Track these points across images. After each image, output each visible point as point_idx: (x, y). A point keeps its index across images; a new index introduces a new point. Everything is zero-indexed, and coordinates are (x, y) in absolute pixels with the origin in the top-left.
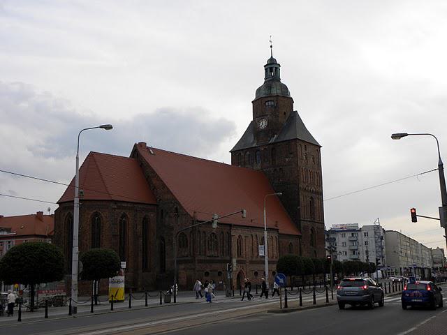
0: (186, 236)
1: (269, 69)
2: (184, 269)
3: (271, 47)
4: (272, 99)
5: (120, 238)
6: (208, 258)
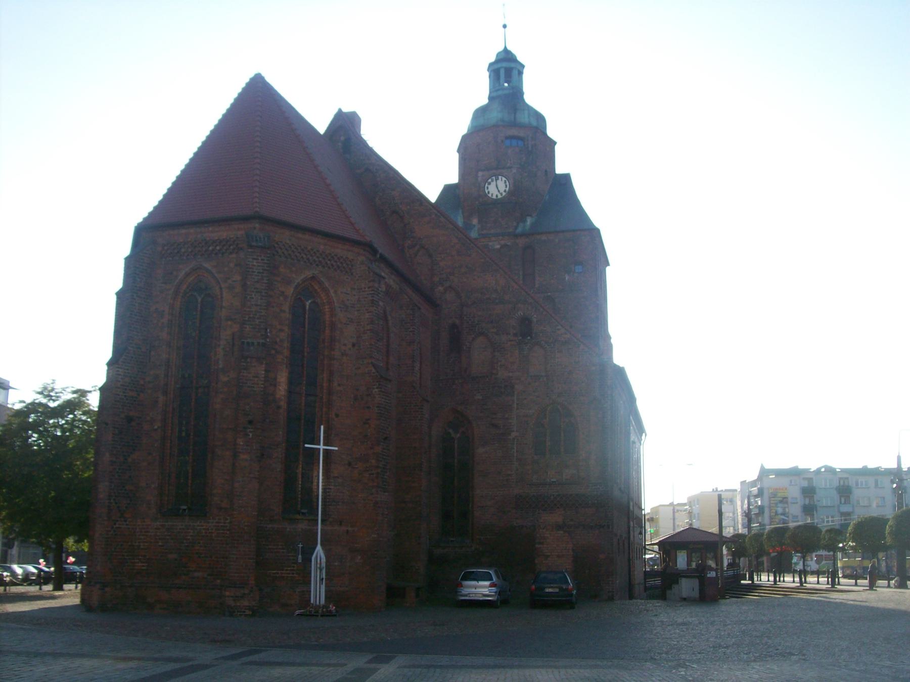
1: (502, 72)
2: (559, 527)
3: (505, 26)
4: (522, 134)
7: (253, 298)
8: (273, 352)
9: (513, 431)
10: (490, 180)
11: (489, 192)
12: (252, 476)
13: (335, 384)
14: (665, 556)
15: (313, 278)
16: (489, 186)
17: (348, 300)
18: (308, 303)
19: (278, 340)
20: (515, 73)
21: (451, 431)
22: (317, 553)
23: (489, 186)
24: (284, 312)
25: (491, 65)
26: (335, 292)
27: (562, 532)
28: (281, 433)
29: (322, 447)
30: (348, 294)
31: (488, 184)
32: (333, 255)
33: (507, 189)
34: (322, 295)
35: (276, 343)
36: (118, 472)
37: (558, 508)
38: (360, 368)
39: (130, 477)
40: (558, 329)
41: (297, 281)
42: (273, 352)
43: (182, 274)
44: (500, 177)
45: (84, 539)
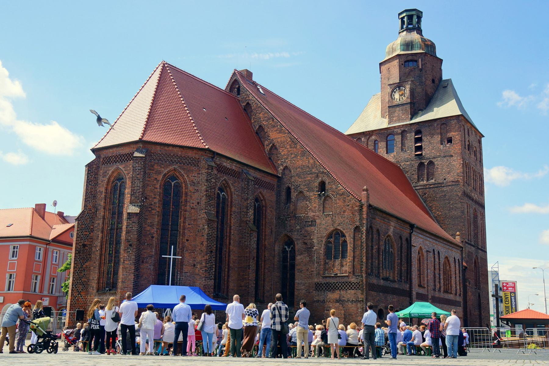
0: (344, 236)
2: (337, 301)
5: (101, 255)
6: (382, 282)
7: (136, 183)
8: (150, 209)
9: (315, 246)
10: (395, 90)
12: (130, 272)
13: (187, 224)
15: (175, 170)
17: (195, 180)
18: (173, 183)
19: (153, 203)
21: (286, 247)
22: (167, 312)
23: (395, 94)
24: (157, 188)
25: (400, 14)
26: (188, 176)
27: (338, 304)
28: (154, 250)
29: (172, 257)
30: (196, 177)
32: (186, 157)
34: (181, 178)
35: (152, 204)
36: (77, 272)
38: (200, 215)
39: (84, 274)
40: (339, 187)
41: (165, 172)
42: (150, 209)
43: (110, 172)
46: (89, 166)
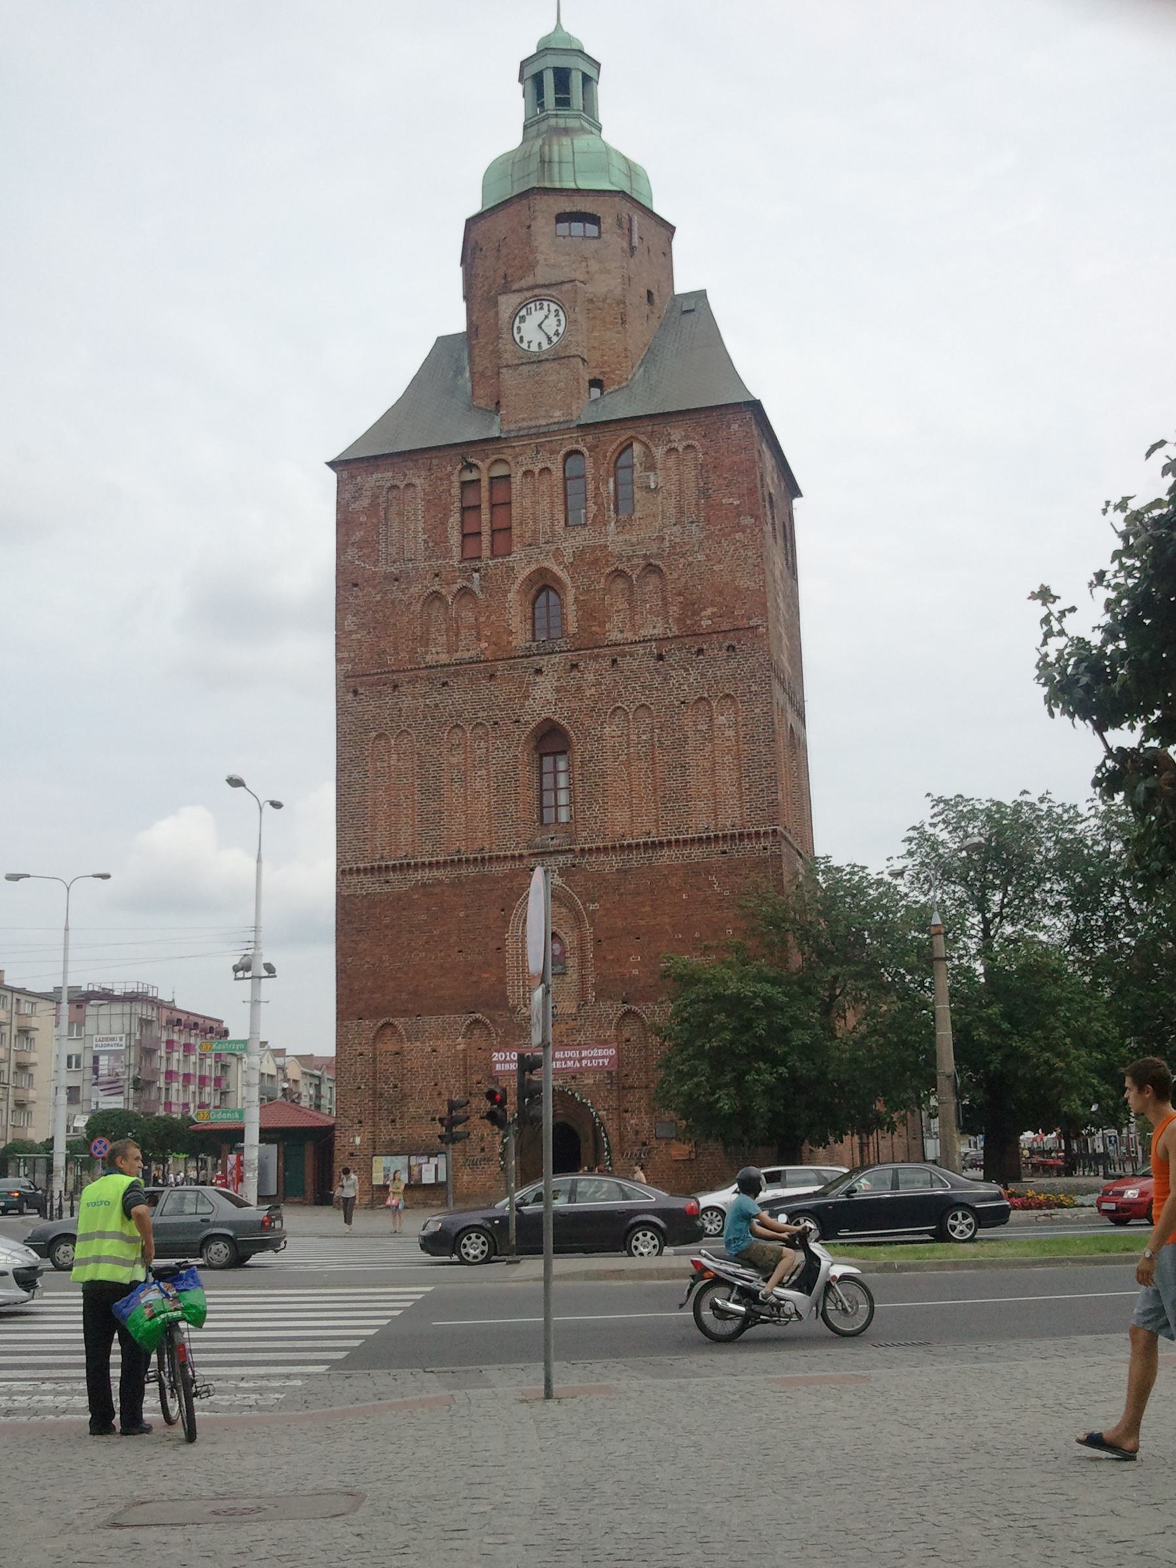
1: (549, 80)
10: (523, 312)
11: (521, 339)
14: (497, 1222)
16: (523, 326)
20: (576, 81)
23: (523, 326)
31: (520, 322)
33: (561, 330)
37: (899, 874)
44: (545, 304)
45: (1121, 791)
46: (443, 343)
